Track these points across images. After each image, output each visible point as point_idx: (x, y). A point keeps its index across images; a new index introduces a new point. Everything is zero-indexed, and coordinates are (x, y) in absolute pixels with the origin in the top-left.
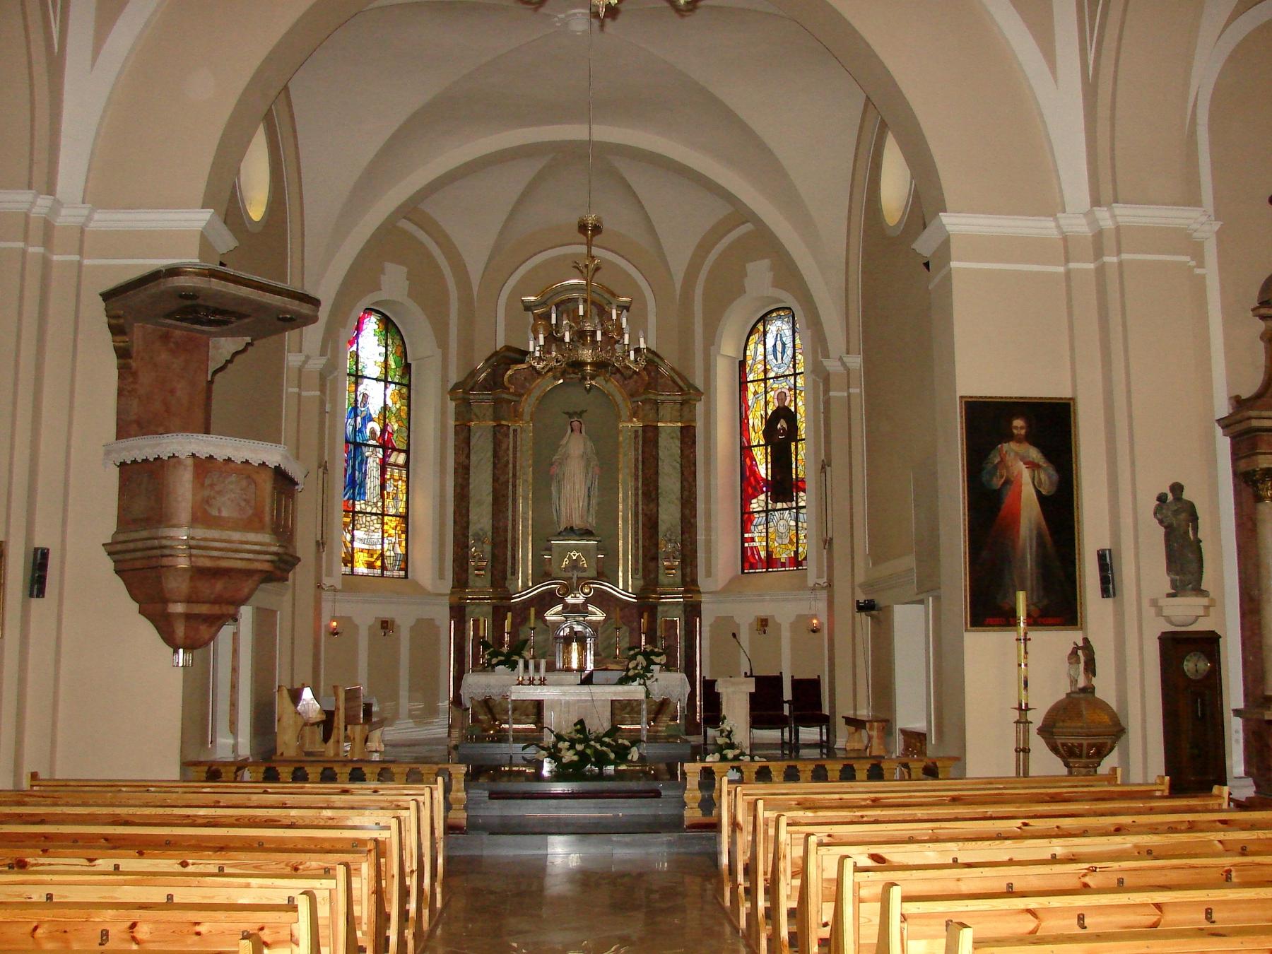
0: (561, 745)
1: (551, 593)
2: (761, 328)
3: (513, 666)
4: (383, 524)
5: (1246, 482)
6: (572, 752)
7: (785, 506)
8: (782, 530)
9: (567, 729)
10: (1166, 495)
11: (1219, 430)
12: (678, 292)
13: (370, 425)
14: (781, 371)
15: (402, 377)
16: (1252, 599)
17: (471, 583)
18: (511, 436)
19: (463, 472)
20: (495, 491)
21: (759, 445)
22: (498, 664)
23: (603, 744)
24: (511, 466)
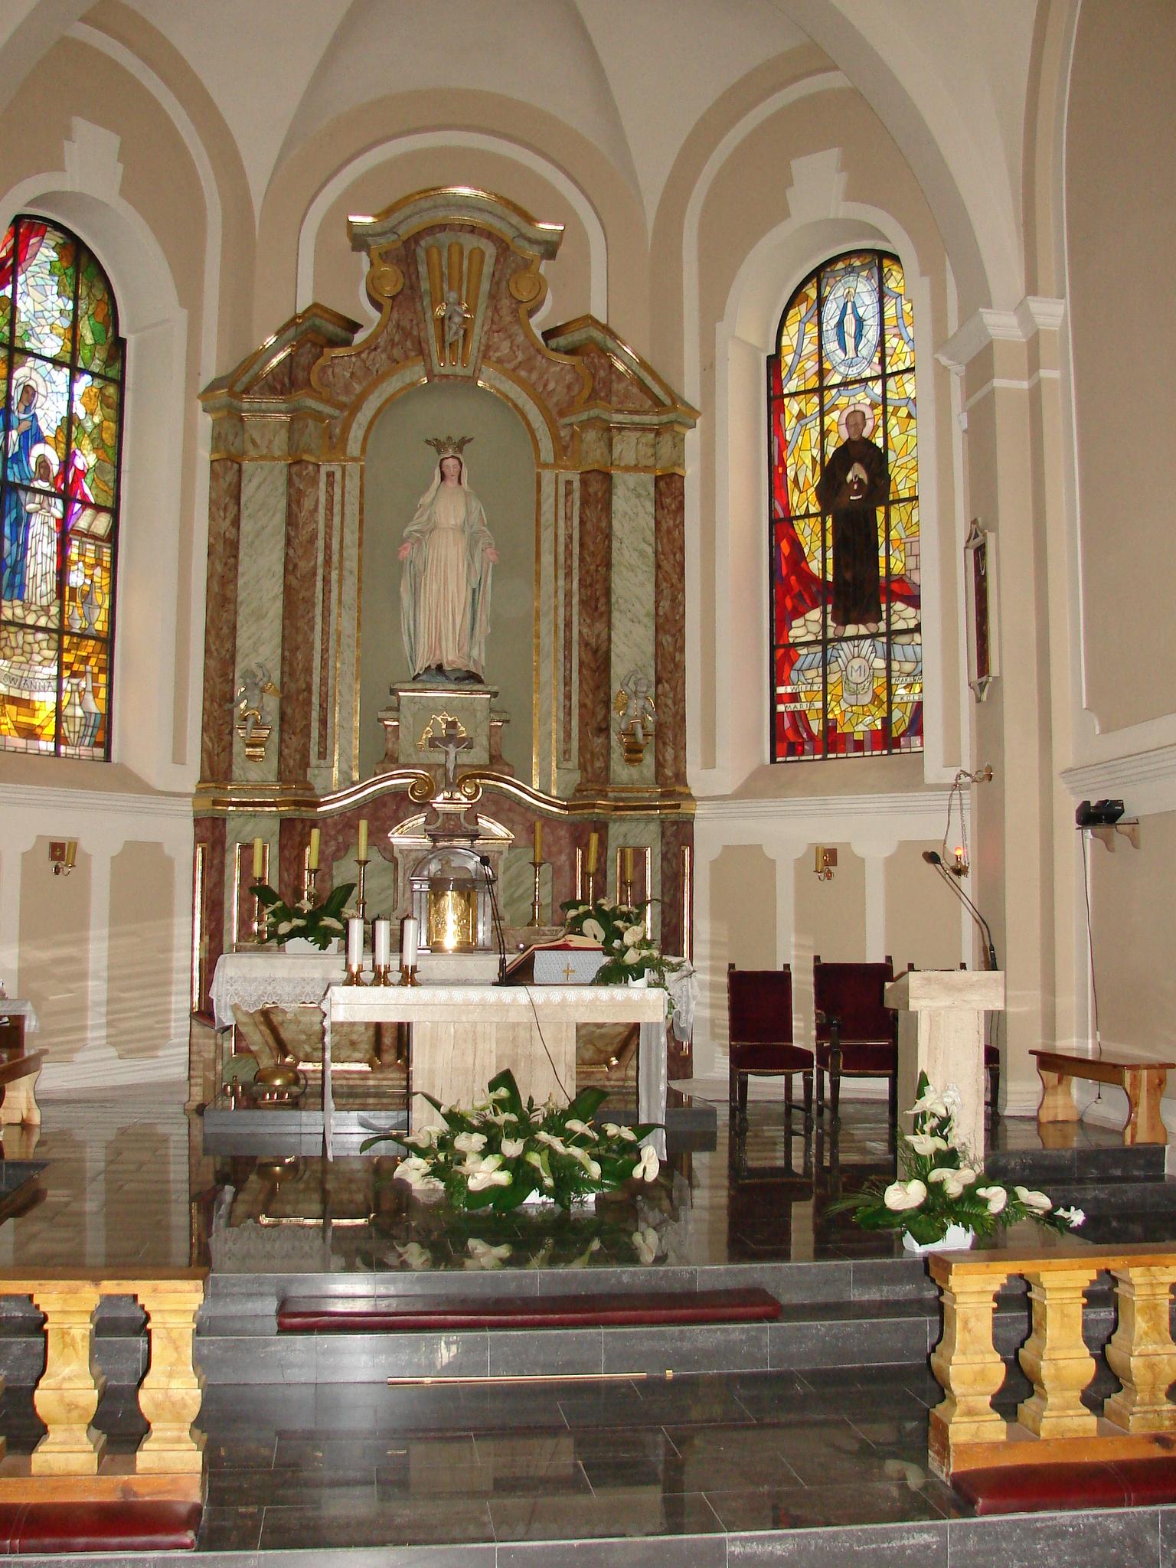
0: (462, 1142)
1: (399, 796)
2: (812, 292)
3: (323, 939)
4: (60, 650)
6: (493, 1161)
7: (863, 630)
8: (855, 677)
9: (474, 1098)
12: (650, 226)
13: (38, 450)
14: (853, 373)
15: (108, 363)
17: (237, 771)
18: (322, 485)
19: (226, 552)
20: (288, 590)
21: (807, 515)
22: (291, 935)
23: (569, 1138)
24: (320, 543)
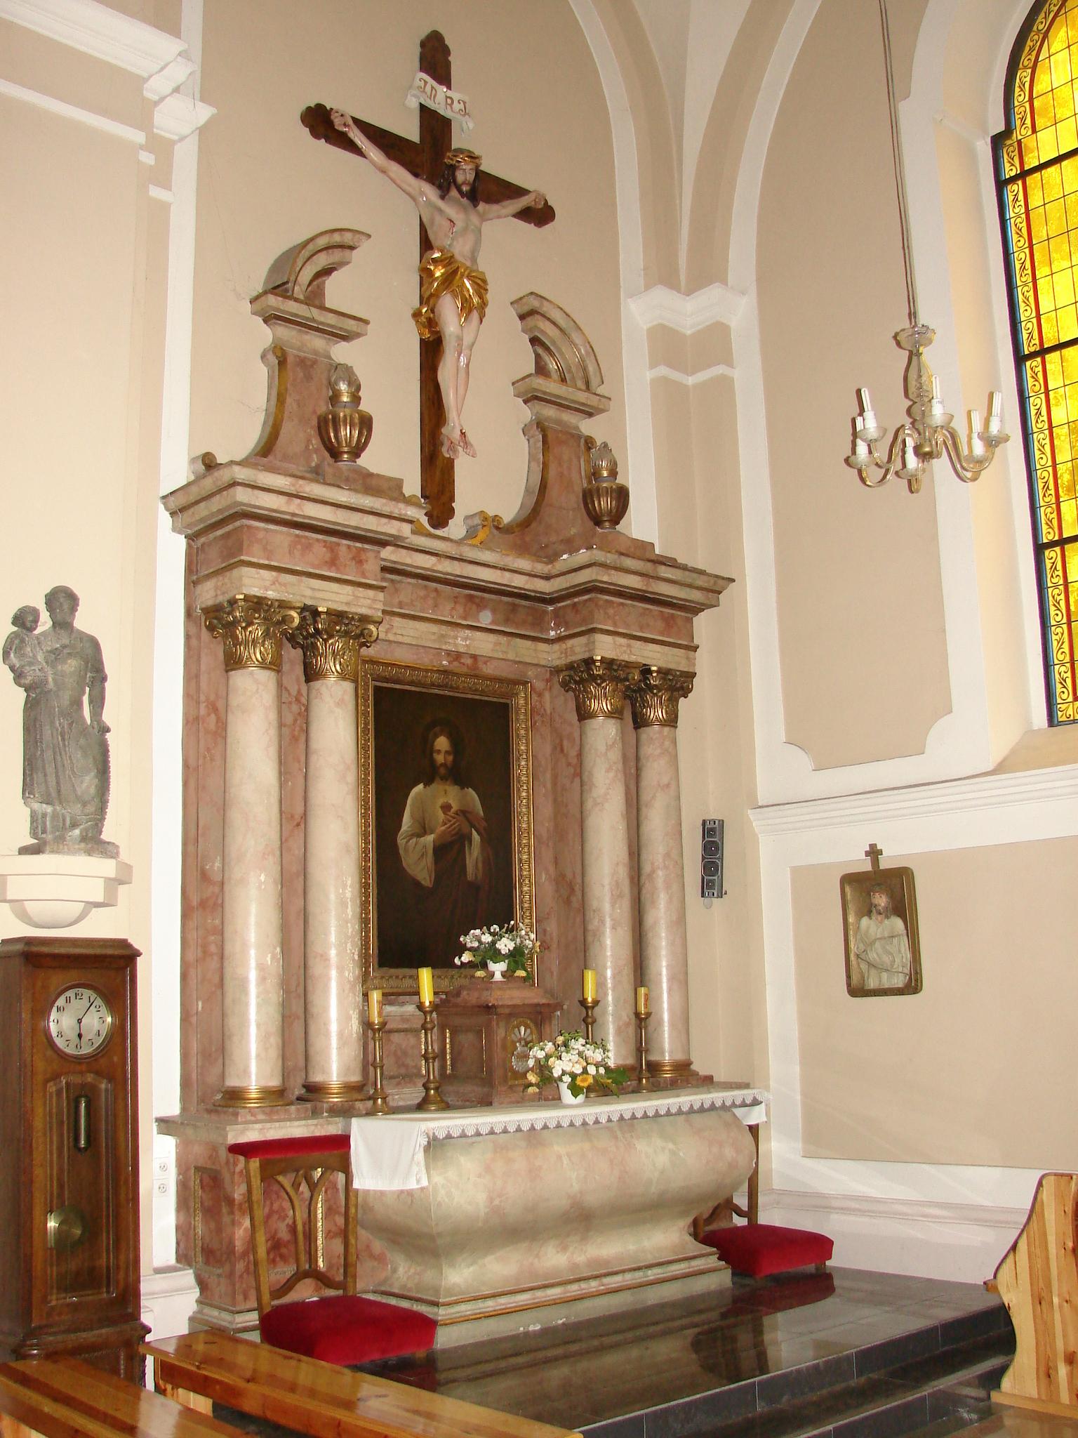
5: (211, 628)
10: (35, 613)
11: (165, 519)
16: (204, 876)
